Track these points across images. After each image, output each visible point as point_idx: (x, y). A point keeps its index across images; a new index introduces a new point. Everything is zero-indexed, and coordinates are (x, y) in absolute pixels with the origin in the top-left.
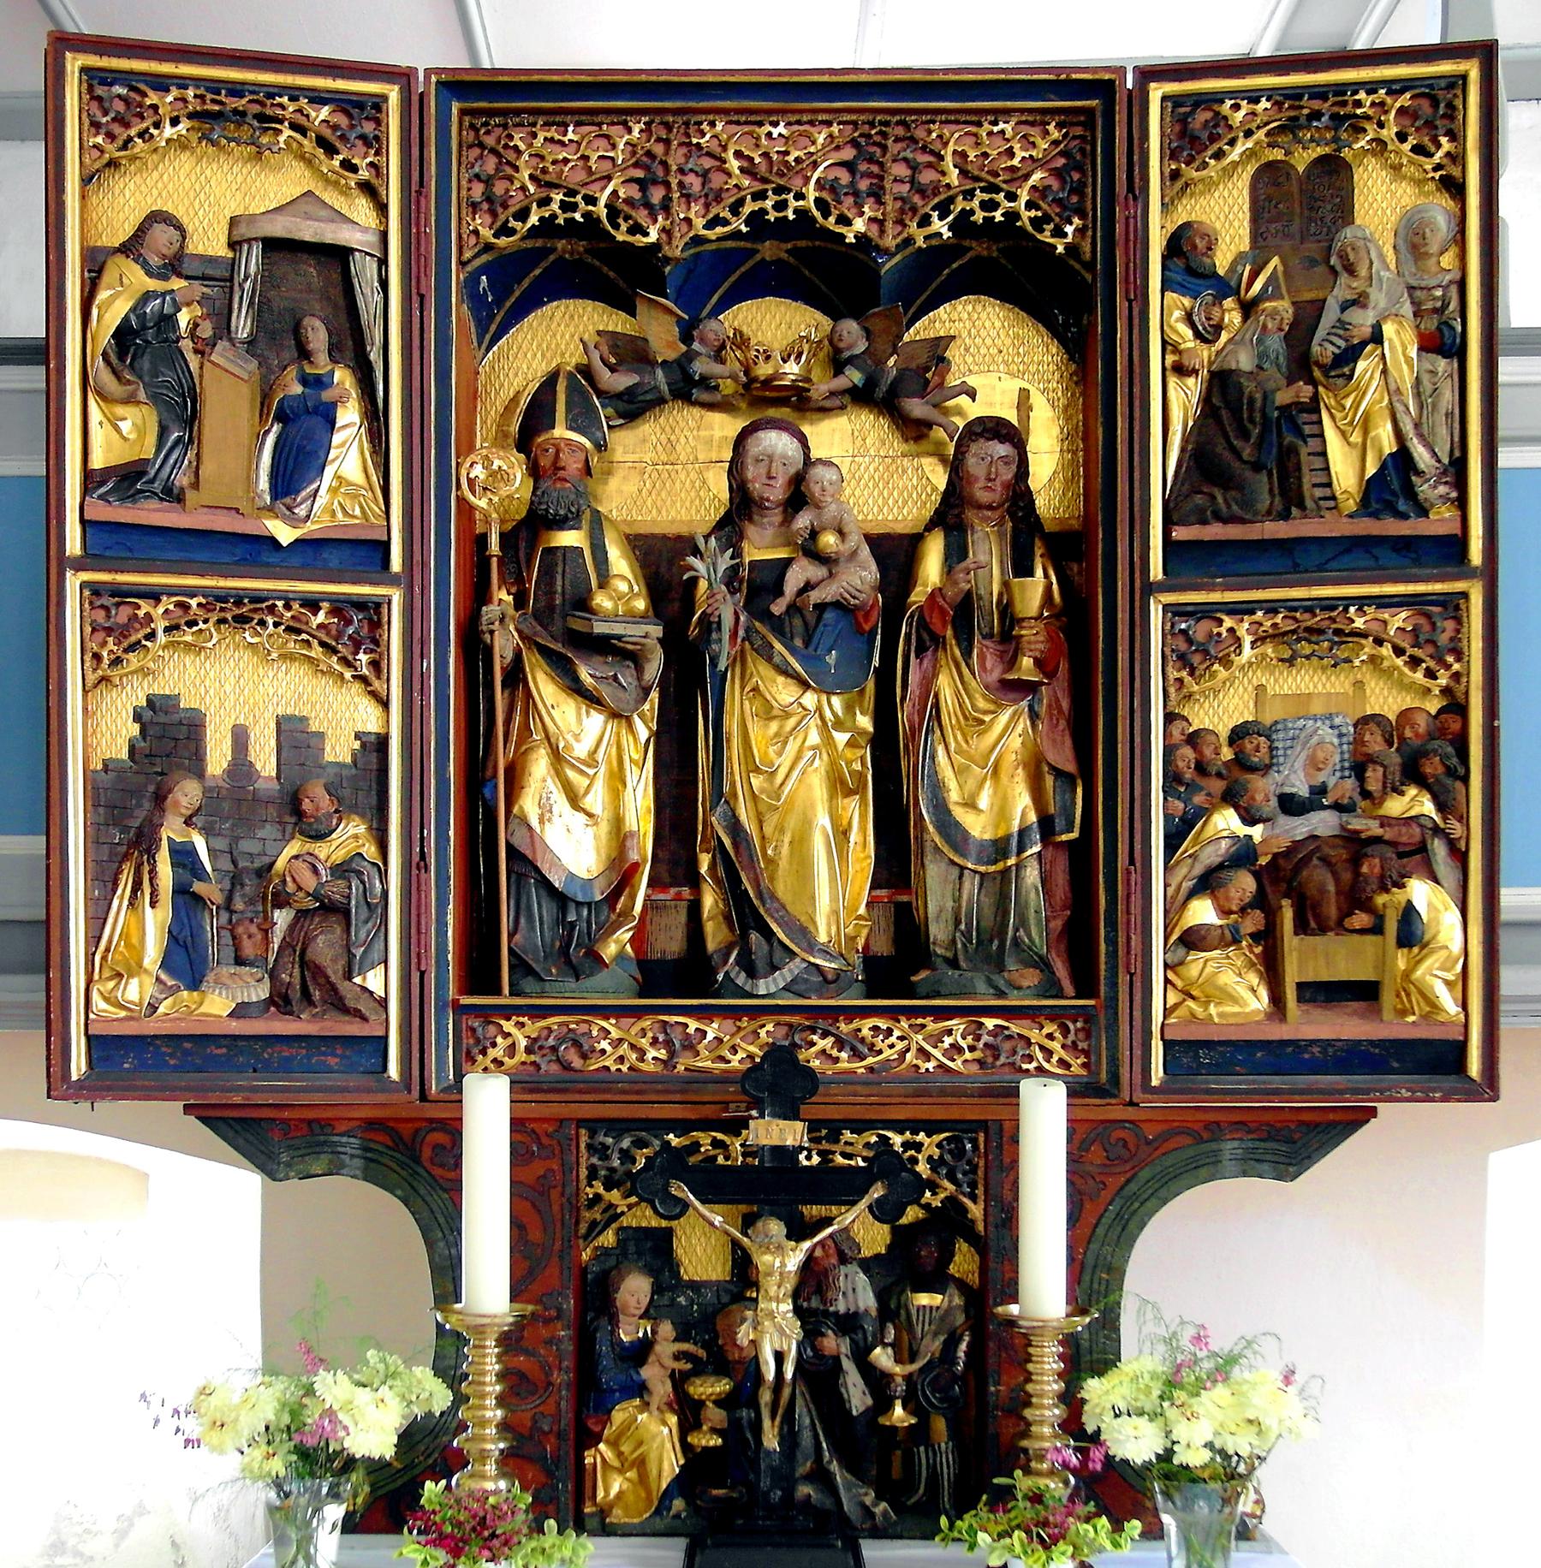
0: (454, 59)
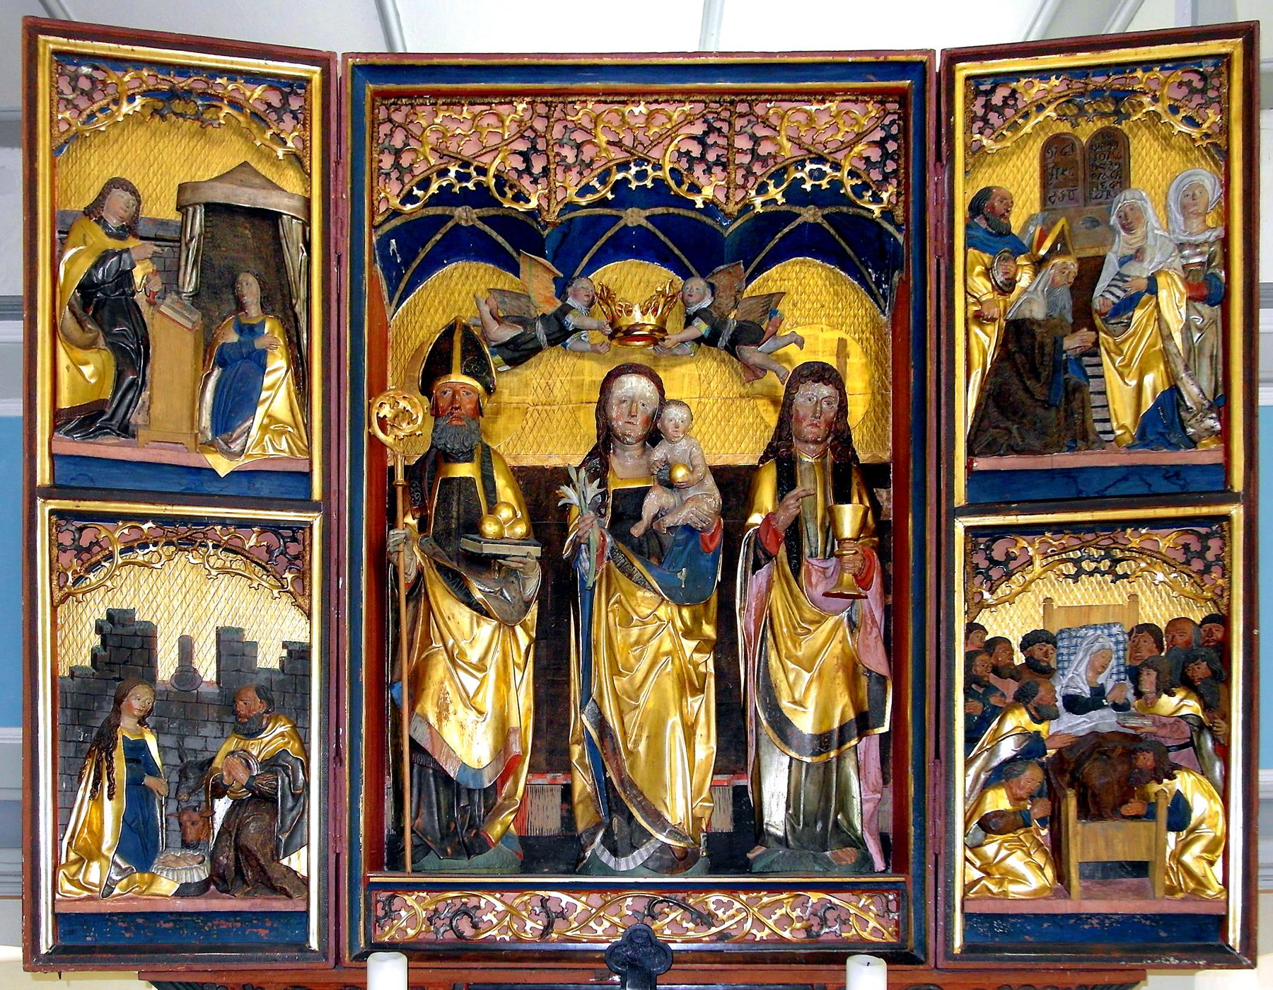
0: (370, 43)
